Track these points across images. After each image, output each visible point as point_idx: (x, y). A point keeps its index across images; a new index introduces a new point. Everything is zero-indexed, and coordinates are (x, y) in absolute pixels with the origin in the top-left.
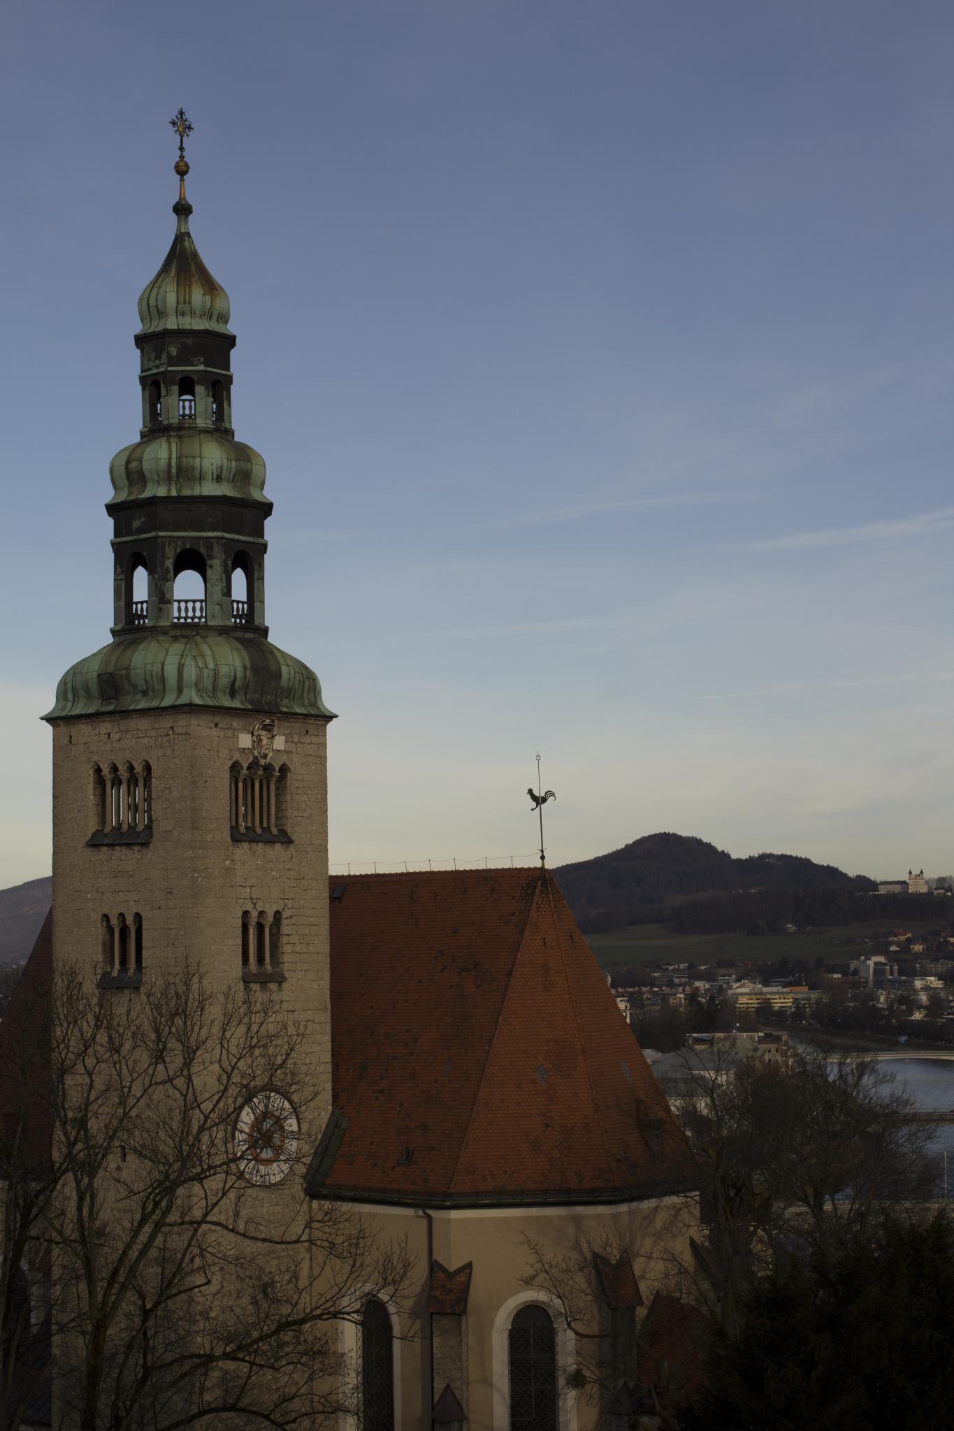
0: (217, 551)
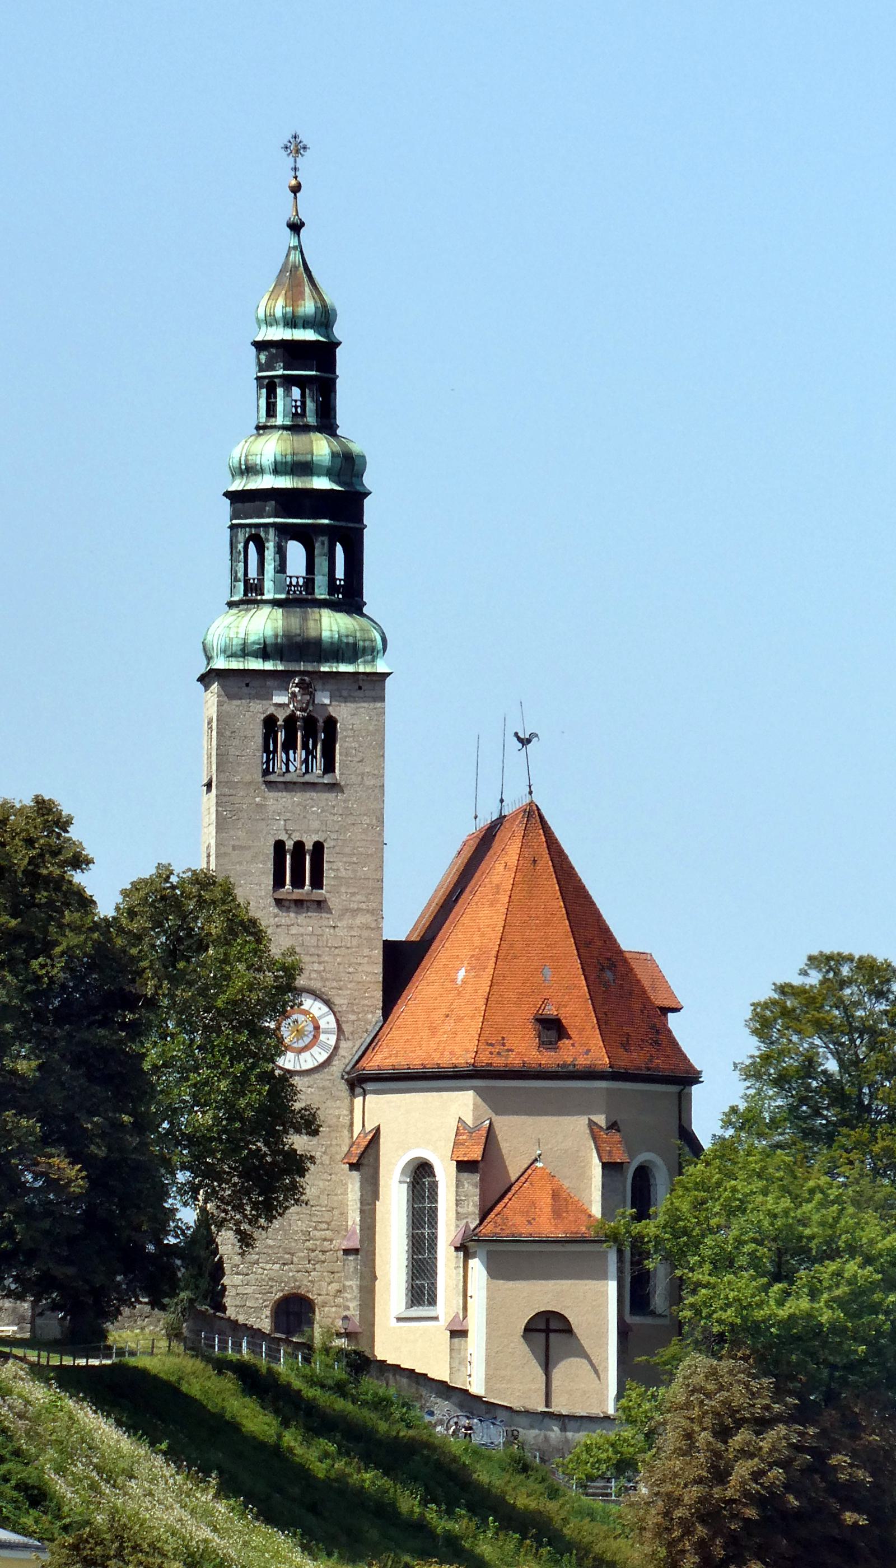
0: (272, 531)
